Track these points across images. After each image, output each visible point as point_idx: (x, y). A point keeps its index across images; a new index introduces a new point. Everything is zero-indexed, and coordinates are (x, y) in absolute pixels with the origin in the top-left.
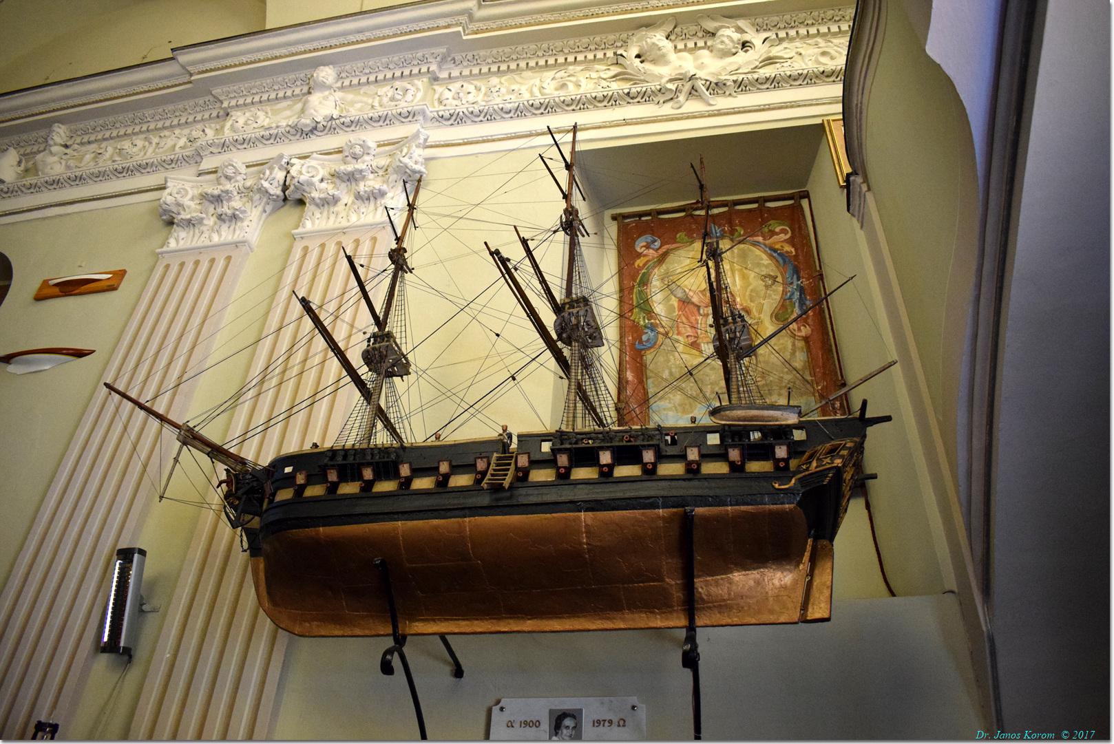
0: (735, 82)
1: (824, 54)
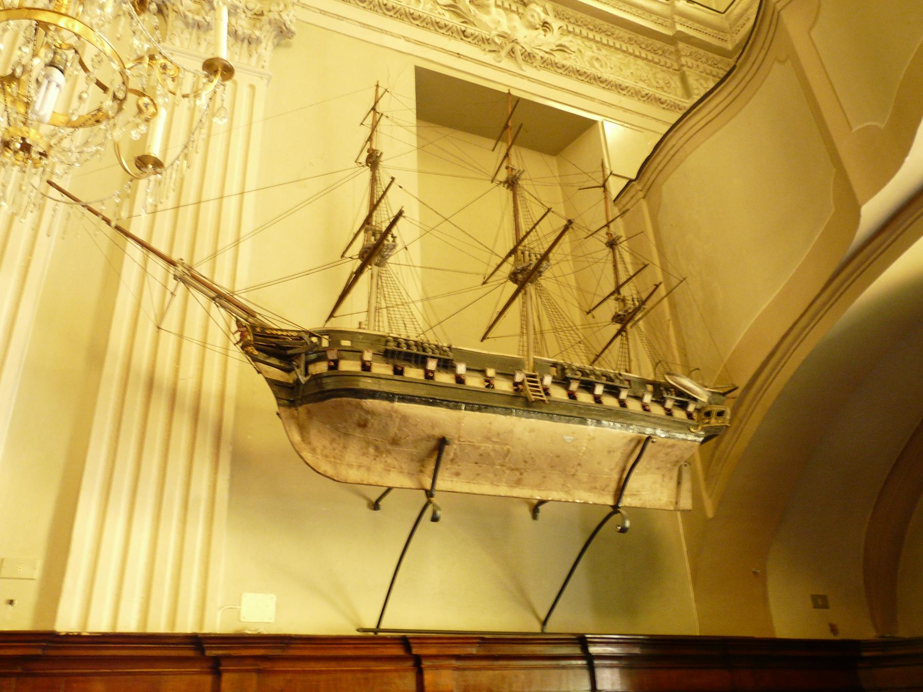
0: (542, 58)
1: (597, 59)
